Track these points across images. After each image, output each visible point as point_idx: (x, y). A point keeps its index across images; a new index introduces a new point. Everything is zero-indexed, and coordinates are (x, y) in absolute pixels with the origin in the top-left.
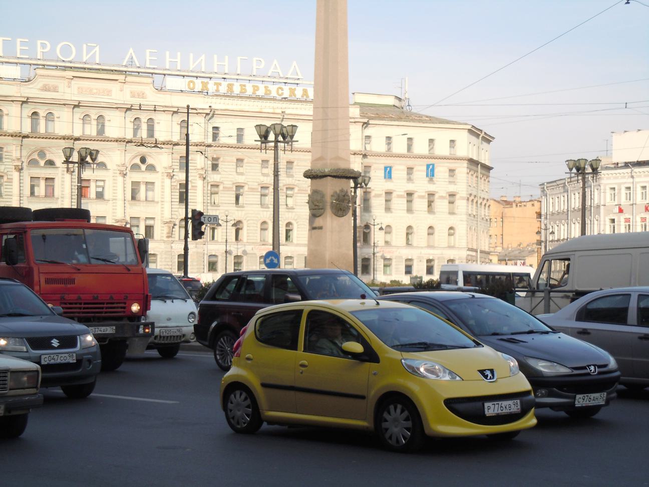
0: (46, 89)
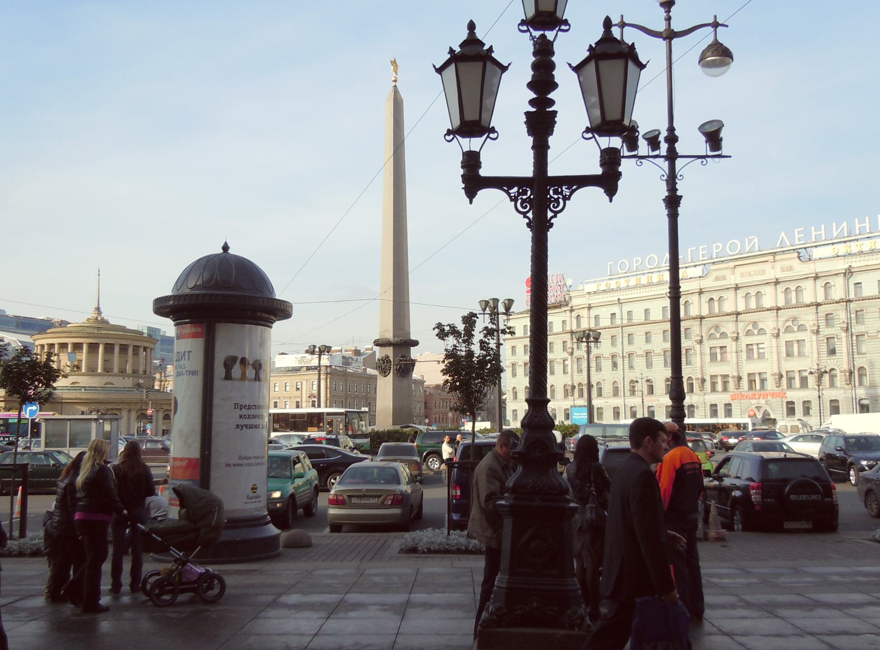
0: (717, 279)
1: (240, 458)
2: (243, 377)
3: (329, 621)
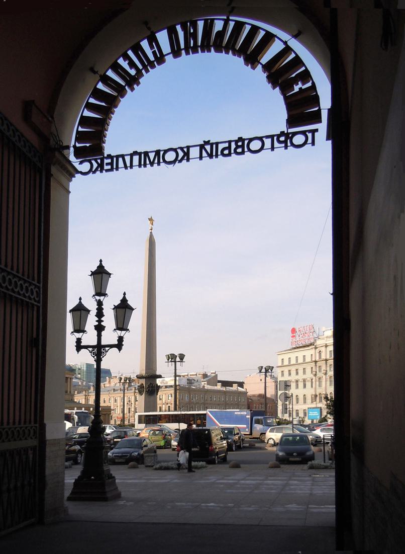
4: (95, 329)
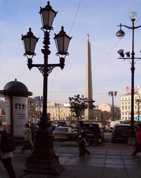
1: (20, 125)
2: (20, 108)
3: (70, 160)
4: (42, 52)
